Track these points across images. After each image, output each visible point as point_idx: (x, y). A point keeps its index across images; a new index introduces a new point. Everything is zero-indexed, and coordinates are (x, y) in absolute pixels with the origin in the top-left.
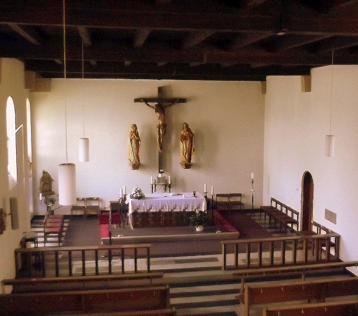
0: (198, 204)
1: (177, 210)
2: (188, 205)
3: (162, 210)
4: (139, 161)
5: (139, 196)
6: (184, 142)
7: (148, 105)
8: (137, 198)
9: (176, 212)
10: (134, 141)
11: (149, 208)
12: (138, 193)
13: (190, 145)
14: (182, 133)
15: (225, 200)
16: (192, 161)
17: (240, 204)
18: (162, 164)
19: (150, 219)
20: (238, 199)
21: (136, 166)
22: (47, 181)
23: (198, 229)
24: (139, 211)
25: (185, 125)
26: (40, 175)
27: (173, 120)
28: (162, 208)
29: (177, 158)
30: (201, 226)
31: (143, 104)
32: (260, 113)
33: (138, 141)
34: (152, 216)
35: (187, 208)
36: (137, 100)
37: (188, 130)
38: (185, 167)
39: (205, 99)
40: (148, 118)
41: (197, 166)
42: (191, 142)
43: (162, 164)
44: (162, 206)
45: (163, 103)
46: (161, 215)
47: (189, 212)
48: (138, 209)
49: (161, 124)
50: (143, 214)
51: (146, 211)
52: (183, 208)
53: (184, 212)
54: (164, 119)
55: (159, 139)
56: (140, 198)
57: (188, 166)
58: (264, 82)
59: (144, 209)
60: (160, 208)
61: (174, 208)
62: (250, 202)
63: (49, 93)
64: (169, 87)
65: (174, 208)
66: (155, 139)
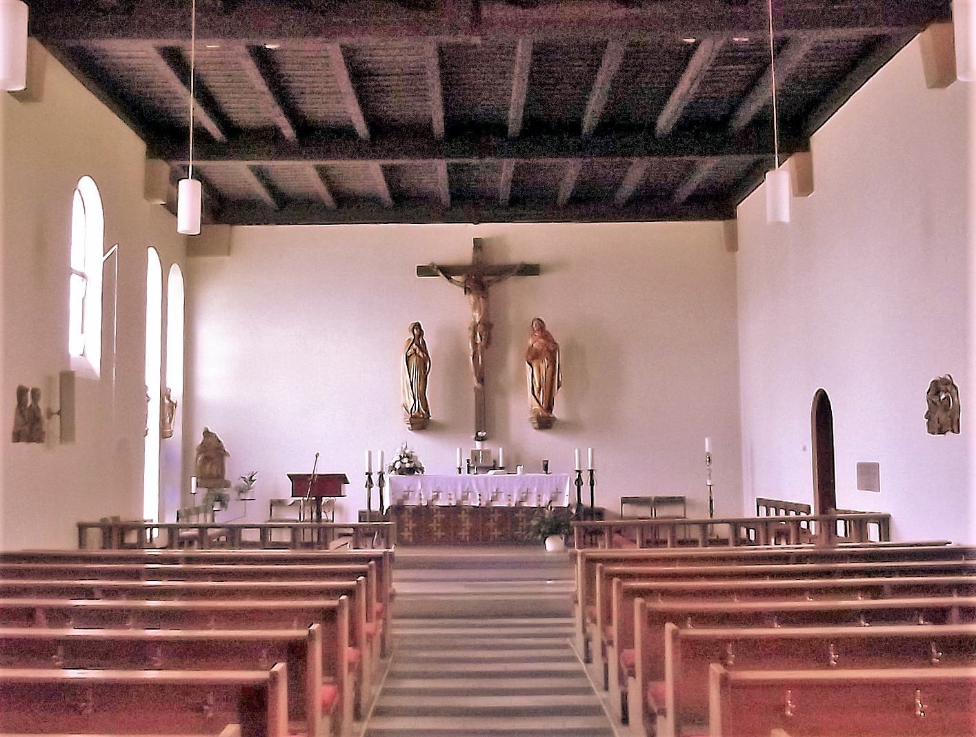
1: (502, 503)
3: (465, 503)
4: (426, 408)
5: (408, 465)
7: (449, 279)
8: (402, 471)
10: (413, 361)
12: (405, 460)
15: (644, 511)
16: (557, 413)
18: (485, 422)
19: (434, 525)
21: (420, 422)
24: (408, 503)
28: (465, 498)
29: (520, 407)
30: (557, 538)
32: (723, 296)
34: (439, 516)
35: (525, 499)
36: (423, 271)
37: (546, 335)
38: (536, 425)
40: (451, 310)
41: (571, 427)
42: (553, 362)
43: (485, 422)
44: (463, 492)
46: (463, 516)
48: (406, 497)
50: (418, 511)
52: (515, 498)
56: (411, 471)
57: (545, 422)
58: (735, 221)
59: (421, 499)
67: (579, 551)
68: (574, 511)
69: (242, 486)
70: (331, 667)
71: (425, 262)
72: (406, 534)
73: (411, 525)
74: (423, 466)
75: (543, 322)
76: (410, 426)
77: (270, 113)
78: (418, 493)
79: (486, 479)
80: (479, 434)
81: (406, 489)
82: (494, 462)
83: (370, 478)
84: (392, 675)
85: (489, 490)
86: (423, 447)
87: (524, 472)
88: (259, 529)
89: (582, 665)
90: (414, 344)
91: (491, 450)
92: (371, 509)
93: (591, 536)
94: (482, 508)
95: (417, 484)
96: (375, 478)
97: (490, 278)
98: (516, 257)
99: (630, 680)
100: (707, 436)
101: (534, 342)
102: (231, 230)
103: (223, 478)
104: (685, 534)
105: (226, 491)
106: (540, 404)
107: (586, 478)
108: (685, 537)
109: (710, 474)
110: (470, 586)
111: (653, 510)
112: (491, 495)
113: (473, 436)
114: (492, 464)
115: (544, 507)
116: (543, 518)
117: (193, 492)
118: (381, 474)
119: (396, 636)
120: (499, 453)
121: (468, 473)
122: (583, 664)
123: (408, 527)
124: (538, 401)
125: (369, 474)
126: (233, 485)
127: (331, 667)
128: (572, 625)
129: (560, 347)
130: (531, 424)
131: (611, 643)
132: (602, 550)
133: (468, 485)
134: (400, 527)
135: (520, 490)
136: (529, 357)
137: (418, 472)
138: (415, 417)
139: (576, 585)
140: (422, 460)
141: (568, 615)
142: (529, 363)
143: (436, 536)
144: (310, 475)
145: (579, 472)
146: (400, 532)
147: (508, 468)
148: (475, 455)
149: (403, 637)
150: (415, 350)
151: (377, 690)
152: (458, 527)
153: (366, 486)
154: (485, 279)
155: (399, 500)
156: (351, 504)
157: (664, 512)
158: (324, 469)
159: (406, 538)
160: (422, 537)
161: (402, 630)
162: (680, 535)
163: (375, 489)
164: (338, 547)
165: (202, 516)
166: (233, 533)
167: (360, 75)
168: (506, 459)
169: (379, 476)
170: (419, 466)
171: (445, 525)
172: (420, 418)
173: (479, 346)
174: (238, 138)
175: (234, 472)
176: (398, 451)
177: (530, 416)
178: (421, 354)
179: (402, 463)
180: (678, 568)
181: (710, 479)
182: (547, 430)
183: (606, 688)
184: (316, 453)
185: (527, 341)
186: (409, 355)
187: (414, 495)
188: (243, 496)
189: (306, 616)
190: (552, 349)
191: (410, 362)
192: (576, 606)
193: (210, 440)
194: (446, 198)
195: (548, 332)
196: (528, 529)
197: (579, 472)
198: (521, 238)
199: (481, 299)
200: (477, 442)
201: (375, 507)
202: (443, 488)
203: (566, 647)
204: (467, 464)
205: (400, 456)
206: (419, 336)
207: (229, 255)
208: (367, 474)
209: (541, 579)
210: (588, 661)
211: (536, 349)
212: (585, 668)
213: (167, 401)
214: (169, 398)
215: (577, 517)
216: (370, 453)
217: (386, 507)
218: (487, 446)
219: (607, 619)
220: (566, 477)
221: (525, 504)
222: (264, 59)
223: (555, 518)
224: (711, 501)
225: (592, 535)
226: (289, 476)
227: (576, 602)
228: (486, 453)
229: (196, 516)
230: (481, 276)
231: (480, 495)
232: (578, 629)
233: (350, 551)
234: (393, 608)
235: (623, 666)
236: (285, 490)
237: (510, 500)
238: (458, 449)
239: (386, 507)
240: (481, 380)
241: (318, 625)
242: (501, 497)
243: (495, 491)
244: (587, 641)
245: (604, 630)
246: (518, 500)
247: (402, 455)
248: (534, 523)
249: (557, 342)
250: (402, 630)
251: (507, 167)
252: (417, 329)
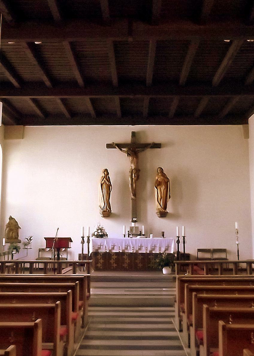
0: (167, 246)
3: (126, 251)
4: (110, 208)
5: (100, 233)
7: (121, 150)
8: (98, 236)
10: (104, 186)
11: (112, 248)
12: (99, 231)
13: (165, 190)
15: (208, 256)
16: (169, 210)
18: (136, 213)
19: (112, 261)
20: (223, 255)
21: (107, 213)
22: (13, 228)
23: (165, 271)
24: (99, 251)
26: (7, 221)
27: (148, 165)
29: (153, 207)
30: (168, 268)
31: (117, 149)
34: (114, 257)
35: (154, 249)
36: (109, 146)
39: (183, 145)
40: (121, 164)
41: (175, 216)
42: (167, 187)
43: (136, 213)
45: (135, 148)
46: (125, 257)
48: (100, 248)
49: (133, 168)
52: (149, 249)
54: (137, 163)
55: (132, 185)
57: (163, 214)
58: (247, 125)
59: (106, 249)
60: (124, 249)
61: (140, 249)
63: (22, 140)
64: (144, 132)
65: (140, 249)
67: (177, 276)
68: (176, 255)
69: (26, 243)
70: (64, 321)
71: (110, 142)
72: (99, 265)
73: (101, 261)
74: (107, 234)
75: (162, 169)
76: (102, 215)
77: (40, 75)
78: (105, 246)
79: (136, 240)
80: (133, 219)
82: (140, 232)
83: (83, 239)
84: (87, 338)
85: (137, 245)
86: (108, 225)
87: (153, 237)
88: (29, 264)
89: (178, 333)
90: (105, 179)
91: (138, 227)
92: (84, 253)
93: (184, 267)
94: (134, 253)
95: (104, 242)
96: (86, 239)
97: (138, 149)
98: (150, 140)
99: (201, 346)
101: (159, 178)
102: (24, 128)
103: (18, 238)
104: (226, 266)
105: (19, 245)
106: (161, 206)
107: (181, 240)
108: (226, 267)
109: (237, 239)
110: (128, 291)
111: (212, 255)
112: (138, 247)
113: (131, 220)
114: (139, 233)
115: (162, 253)
117: (4, 245)
118: (88, 237)
119: (89, 316)
121: (129, 237)
122: (178, 332)
125: (83, 237)
126: (22, 242)
127: (64, 321)
128: (174, 311)
129: (170, 180)
130: (157, 215)
131: (191, 325)
132: (187, 275)
133: (127, 243)
134: (97, 262)
136: (156, 185)
137: (105, 236)
138: (105, 211)
139: (176, 291)
140: (107, 231)
141: (171, 306)
142: (156, 187)
144: (54, 238)
145: (179, 237)
146: (96, 264)
147: (146, 235)
148: (132, 228)
149: (93, 317)
150: (105, 181)
151: (77, 346)
153: (81, 243)
154: (137, 150)
155: (96, 249)
156: (75, 251)
157: (216, 256)
158: (61, 235)
160: (106, 267)
161: (93, 312)
162: (225, 266)
163: (86, 244)
164: (67, 272)
165: (6, 257)
166: (17, 266)
167: (78, 57)
168: (146, 231)
169: (87, 238)
170: (105, 234)
172: (107, 212)
173: (134, 180)
174: (27, 87)
175: (23, 236)
176: (96, 227)
178: (108, 183)
179: (98, 232)
180: (224, 286)
181: (238, 241)
182: (165, 218)
183: (189, 347)
184: (57, 228)
185: (155, 178)
186: (102, 183)
187: (103, 247)
188: (26, 247)
189: (66, 288)
190: (166, 181)
192: (175, 303)
193: (12, 221)
197: (179, 237)
199: (135, 159)
200: (132, 223)
201: (85, 252)
202: (116, 244)
203: (171, 323)
204: (128, 233)
205: (97, 229)
206: (107, 175)
207: (23, 138)
208: (82, 237)
209: (160, 288)
210: (181, 331)
211: (160, 181)
212: (179, 334)
215: (178, 259)
217: (90, 253)
219: (190, 312)
220: (172, 240)
222: (36, 50)
223: (167, 258)
224: (238, 251)
225: (183, 268)
226: (44, 238)
227: (176, 301)
228: (137, 228)
229: (4, 256)
231: (133, 247)
232: (176, 314)
233: (71, 275)
234: (90, 302)
235: (197, 339)
236: (43, 244)
237: (146, 250)
238: (124, 226)
239: (90, 253)
240: (135, 195)
241: (59, 302)
242: (142, 248)
243: (140, 245)
244: (181, 321)
245: (188, 318)
247: (98, 229)
248: (157, 261)
249: (169, 178)
250: (93, 312)
251: (146, 99)
252: (106, 172)
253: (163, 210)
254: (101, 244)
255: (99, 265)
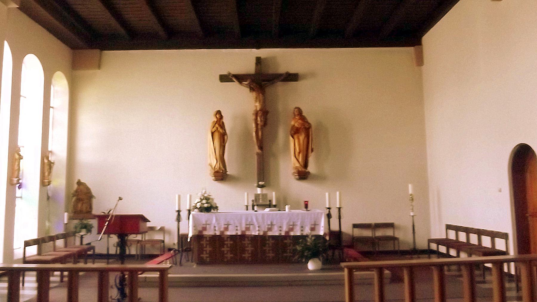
1: (275, 232)
2: (293, 225)
3: (248, 233)
4: (224, 166)
5: (206, 205)
6: (295, 136)
8: (202, 209)
9: (273, 237)
10: (217, 136)
12: (204, 201)
14: (293, 123)
15: (367, 233)
16: (312, 168)
17: (394, 239)
18: (264, 174)
19: (225, 249)
20: (389, 232)
21: (221, 175)
24: (205, 233)
25: (296, 110)
27: (280, 107)
28: (248, 229)
29: (287, 165)
30: (316, 260)
31: (235, 85)
32: (415, 96)
33: (223, 137)
34: (229, 242)
36: (224, 78)
39: (330, 78)
40: (241, 103)
41: (320, 178)
42: (308, 136)
43: (264, 174)
46: (246, 242)
47: (296, 238)
48: (205, 229)
49: (258, 109)
50: (214, 238)
51: (218, 233)
52: (285, 229)
53: (287, 236)
56: (208, 210)
57: (303, 175)
59: (215, 230)
60: (244, 229)
61: (270, 229)
62: (409, 238)
64: (273, 58)
65: (270, 229)
66: (252, 134)
73: (208, 249)
78: (214, 225)
79: (263, 215)
81: (204, 223)
87: (291, 209)
95: (212, 219)
98: (283, 69)
100: (410, 183)
102: (101, 54)
113: (256, 185)
116: (306, 245)
120: (273, 196)
123: (206, 251)
124: (298, 161)
133: (250, 220)
135: (288, 223)
140: (217, 201)
143: (227, 257)
145: (329, 208)
148: (257, 196)
150: (217, 128)
152: (243, 251)
159: (205, 258)
168: (278, 200)
171: (233, 249)
176: (199, 195)
177: (293, 171)
182: (305, 181)
191: (214, 137)
193: (81, 187)
194: (237, 29)
195: (304, 116)
196: (295, 251)
198: (287, 58)
199: (261, 95)
202: (232, 222)
213: (46, 161)
214: (48, 158)
216: (191, 196)
218: (265, 191)
221: (292, 234)
228: (264, 196)
230: (261, 81)
231: (259, 227)
240: (261, 148)
243: (269, 223)
246: (287, 230)
248: (299, 248)
253: (303, 170)
254: (206, 221)
255: (204, 256)
